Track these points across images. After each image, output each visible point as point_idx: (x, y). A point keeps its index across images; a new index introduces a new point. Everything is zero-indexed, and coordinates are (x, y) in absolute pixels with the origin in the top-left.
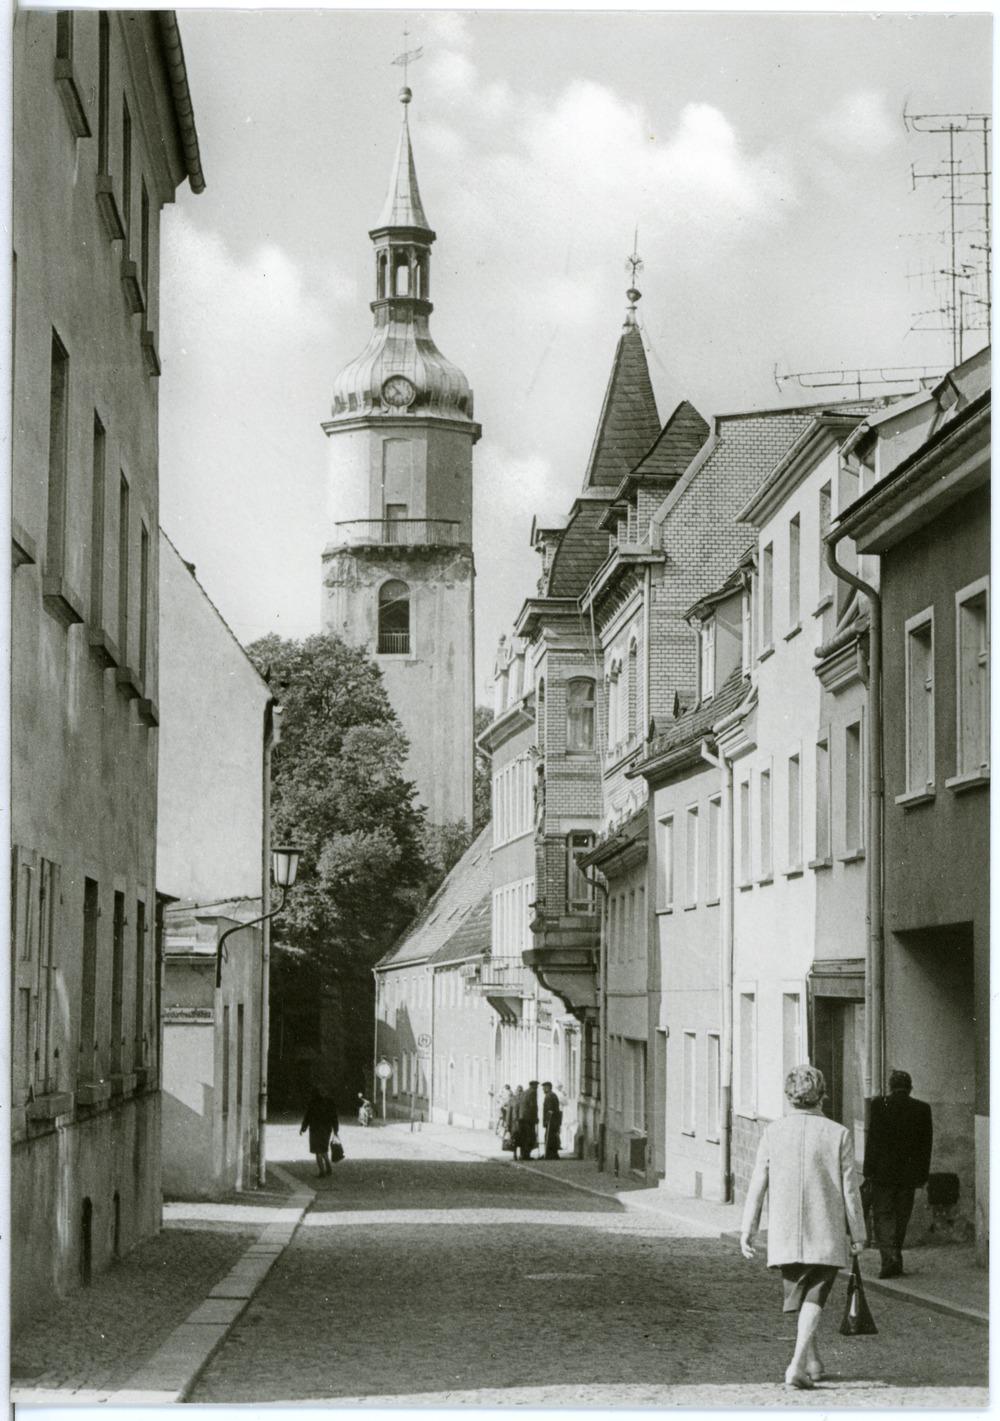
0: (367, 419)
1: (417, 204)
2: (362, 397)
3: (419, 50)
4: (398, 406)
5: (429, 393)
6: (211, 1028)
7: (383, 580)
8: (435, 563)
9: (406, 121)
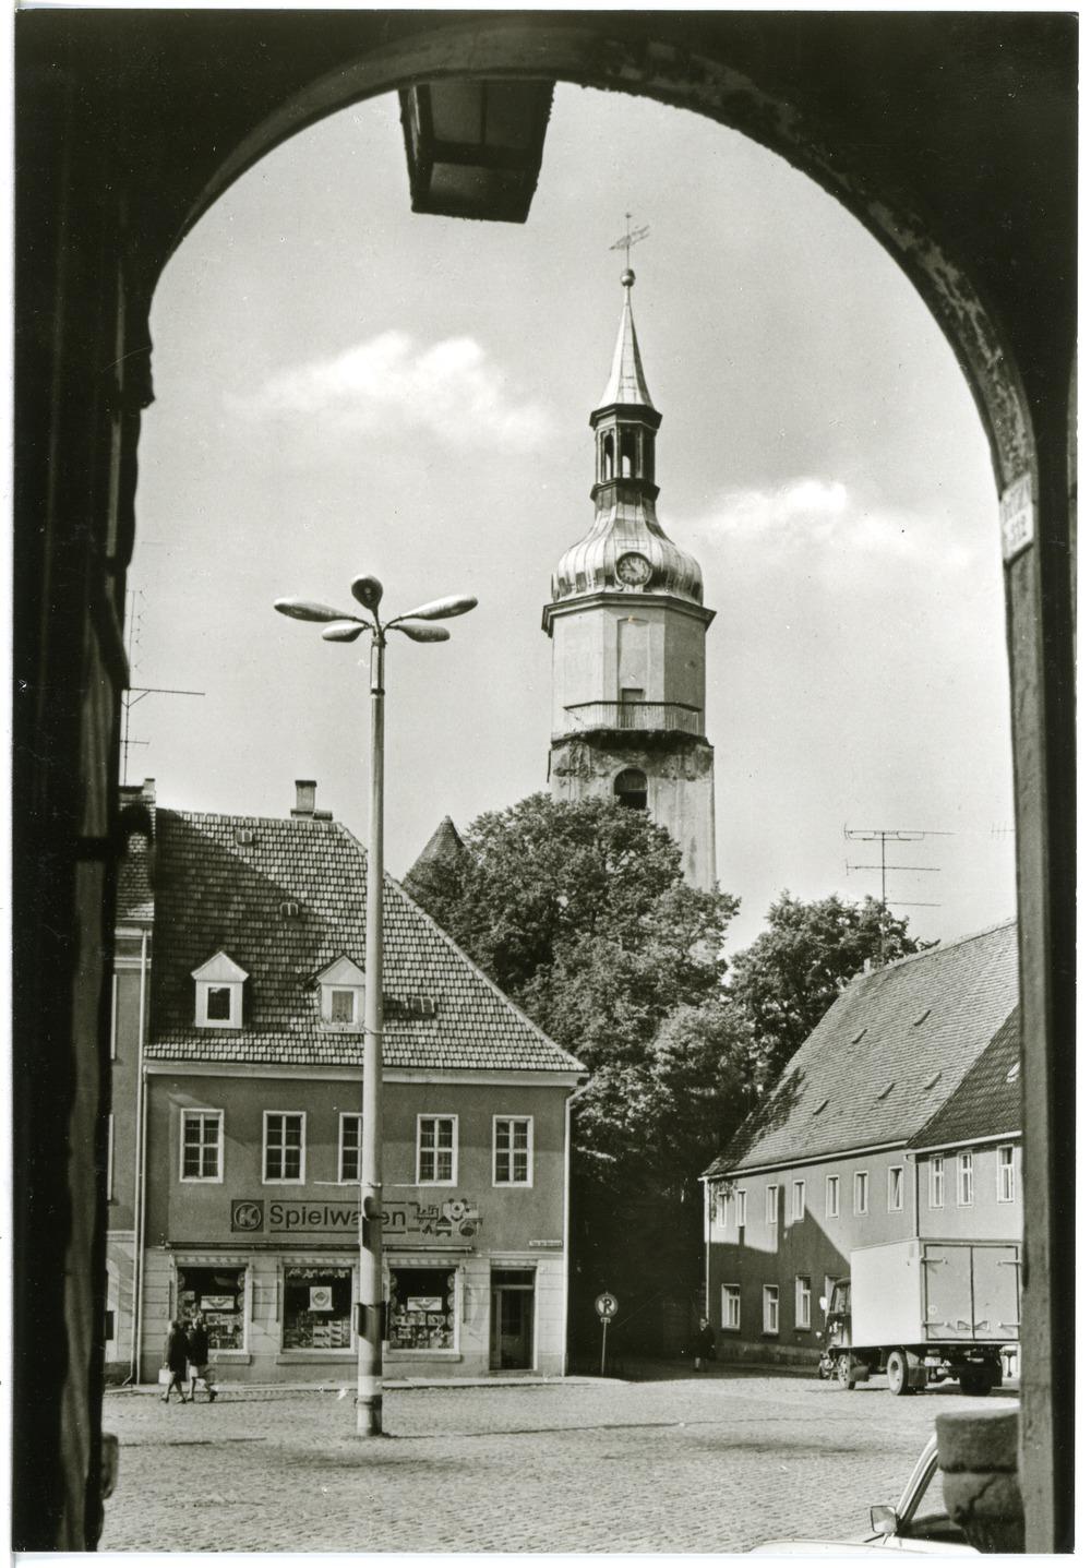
0: (602, 596)
1: (643, 387)
2: (592, 575)
3: (645, 229)
4: (634, 584)
5: (665, 573)
6: (1014, 1250)
7: (620, 769)
8: (675, 754)
9: (629, 304)
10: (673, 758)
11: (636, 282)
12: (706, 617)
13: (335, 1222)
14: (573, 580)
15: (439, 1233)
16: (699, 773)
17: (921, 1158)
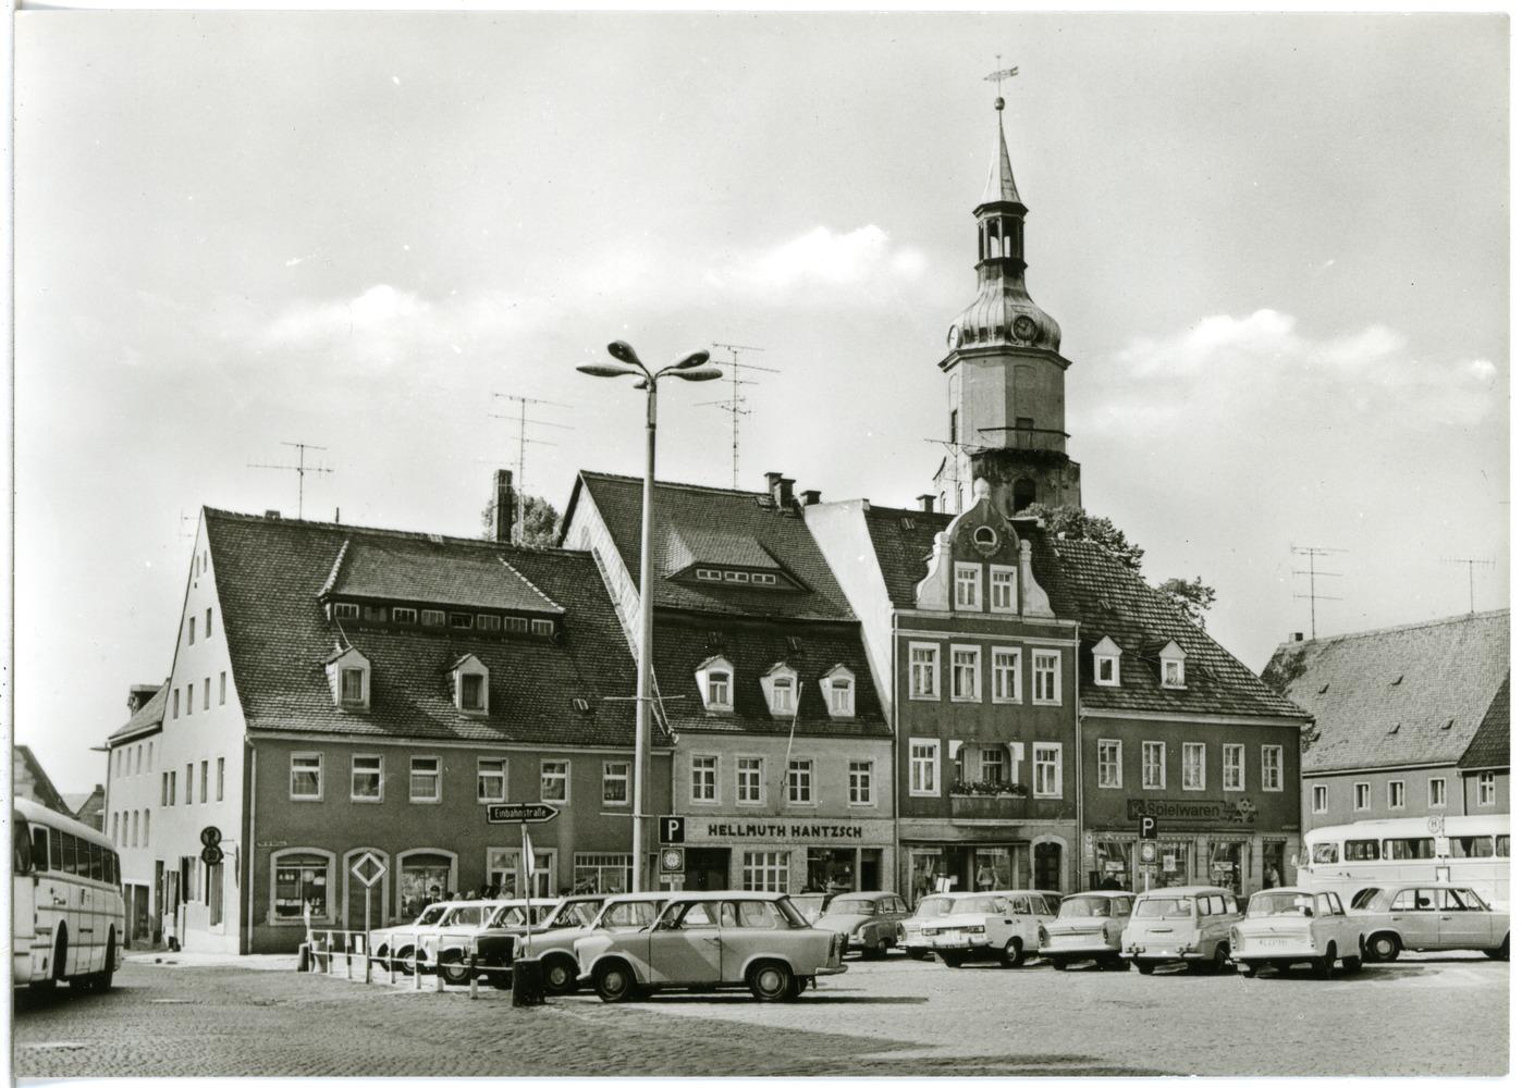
0: (1003, 348)
8: (1054, 468)
10: (1053, 471)
11: (1006, 108)
12: (1065, 364)
13: (1182, 814)
14: (976, 331)
15: (1236, 820)
16: (1071, 483)
17: (1466, 775)
